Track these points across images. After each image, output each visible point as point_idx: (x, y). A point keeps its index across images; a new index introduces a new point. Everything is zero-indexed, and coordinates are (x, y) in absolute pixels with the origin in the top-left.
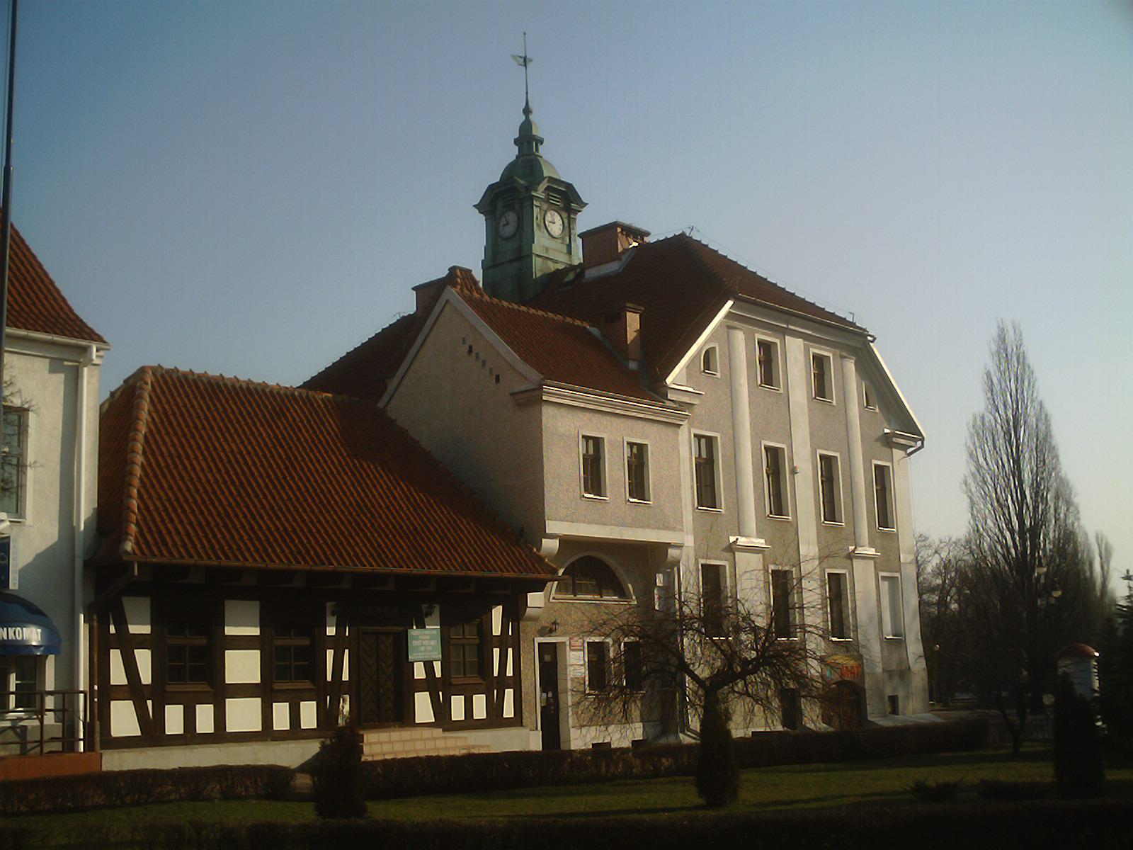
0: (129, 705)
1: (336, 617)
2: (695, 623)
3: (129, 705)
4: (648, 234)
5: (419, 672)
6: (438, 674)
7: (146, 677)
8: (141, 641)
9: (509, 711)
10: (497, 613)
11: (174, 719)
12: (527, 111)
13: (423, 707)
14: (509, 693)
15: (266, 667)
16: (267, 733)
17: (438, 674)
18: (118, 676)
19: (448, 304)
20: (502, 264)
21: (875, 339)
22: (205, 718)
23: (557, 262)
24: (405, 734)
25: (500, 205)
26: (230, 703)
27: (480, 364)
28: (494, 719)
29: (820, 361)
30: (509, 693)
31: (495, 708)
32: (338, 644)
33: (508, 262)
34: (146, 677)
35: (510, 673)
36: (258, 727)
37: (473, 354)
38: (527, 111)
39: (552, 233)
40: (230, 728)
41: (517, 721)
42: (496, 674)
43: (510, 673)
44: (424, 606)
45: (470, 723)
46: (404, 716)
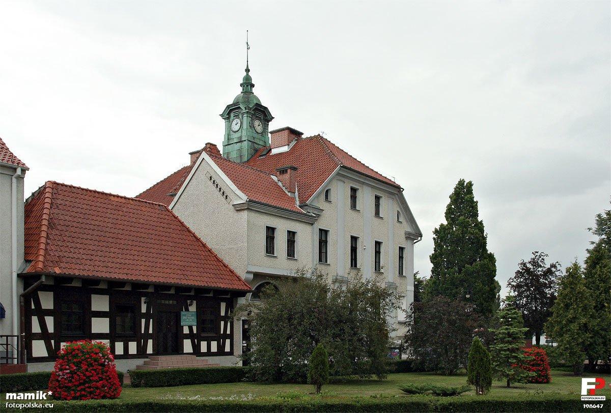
5: (186, 331)
6: (195, 332)
8: (49, 313)
9: (227, 349)
10: (223, 306)
12: (247, 70)
13: (188, 346)
14: (228, 342)
15: (112, 325)
17: (195, 332)
18: (36, 328)
23: (259, 145)
25: (232, 115)
28: (221, 352)
29: (377, 198)
30: (228, 342)
31: (221, 348)
32: (147, 316)
35: (228, 332)
37: (222, 191)
38: (247, 70)
39: (257, 130)
41: (231, 353)
42: (222, 333)
43: (228, 332)
44: (188, 301)
45: (209, 353)
46: (177, 350)
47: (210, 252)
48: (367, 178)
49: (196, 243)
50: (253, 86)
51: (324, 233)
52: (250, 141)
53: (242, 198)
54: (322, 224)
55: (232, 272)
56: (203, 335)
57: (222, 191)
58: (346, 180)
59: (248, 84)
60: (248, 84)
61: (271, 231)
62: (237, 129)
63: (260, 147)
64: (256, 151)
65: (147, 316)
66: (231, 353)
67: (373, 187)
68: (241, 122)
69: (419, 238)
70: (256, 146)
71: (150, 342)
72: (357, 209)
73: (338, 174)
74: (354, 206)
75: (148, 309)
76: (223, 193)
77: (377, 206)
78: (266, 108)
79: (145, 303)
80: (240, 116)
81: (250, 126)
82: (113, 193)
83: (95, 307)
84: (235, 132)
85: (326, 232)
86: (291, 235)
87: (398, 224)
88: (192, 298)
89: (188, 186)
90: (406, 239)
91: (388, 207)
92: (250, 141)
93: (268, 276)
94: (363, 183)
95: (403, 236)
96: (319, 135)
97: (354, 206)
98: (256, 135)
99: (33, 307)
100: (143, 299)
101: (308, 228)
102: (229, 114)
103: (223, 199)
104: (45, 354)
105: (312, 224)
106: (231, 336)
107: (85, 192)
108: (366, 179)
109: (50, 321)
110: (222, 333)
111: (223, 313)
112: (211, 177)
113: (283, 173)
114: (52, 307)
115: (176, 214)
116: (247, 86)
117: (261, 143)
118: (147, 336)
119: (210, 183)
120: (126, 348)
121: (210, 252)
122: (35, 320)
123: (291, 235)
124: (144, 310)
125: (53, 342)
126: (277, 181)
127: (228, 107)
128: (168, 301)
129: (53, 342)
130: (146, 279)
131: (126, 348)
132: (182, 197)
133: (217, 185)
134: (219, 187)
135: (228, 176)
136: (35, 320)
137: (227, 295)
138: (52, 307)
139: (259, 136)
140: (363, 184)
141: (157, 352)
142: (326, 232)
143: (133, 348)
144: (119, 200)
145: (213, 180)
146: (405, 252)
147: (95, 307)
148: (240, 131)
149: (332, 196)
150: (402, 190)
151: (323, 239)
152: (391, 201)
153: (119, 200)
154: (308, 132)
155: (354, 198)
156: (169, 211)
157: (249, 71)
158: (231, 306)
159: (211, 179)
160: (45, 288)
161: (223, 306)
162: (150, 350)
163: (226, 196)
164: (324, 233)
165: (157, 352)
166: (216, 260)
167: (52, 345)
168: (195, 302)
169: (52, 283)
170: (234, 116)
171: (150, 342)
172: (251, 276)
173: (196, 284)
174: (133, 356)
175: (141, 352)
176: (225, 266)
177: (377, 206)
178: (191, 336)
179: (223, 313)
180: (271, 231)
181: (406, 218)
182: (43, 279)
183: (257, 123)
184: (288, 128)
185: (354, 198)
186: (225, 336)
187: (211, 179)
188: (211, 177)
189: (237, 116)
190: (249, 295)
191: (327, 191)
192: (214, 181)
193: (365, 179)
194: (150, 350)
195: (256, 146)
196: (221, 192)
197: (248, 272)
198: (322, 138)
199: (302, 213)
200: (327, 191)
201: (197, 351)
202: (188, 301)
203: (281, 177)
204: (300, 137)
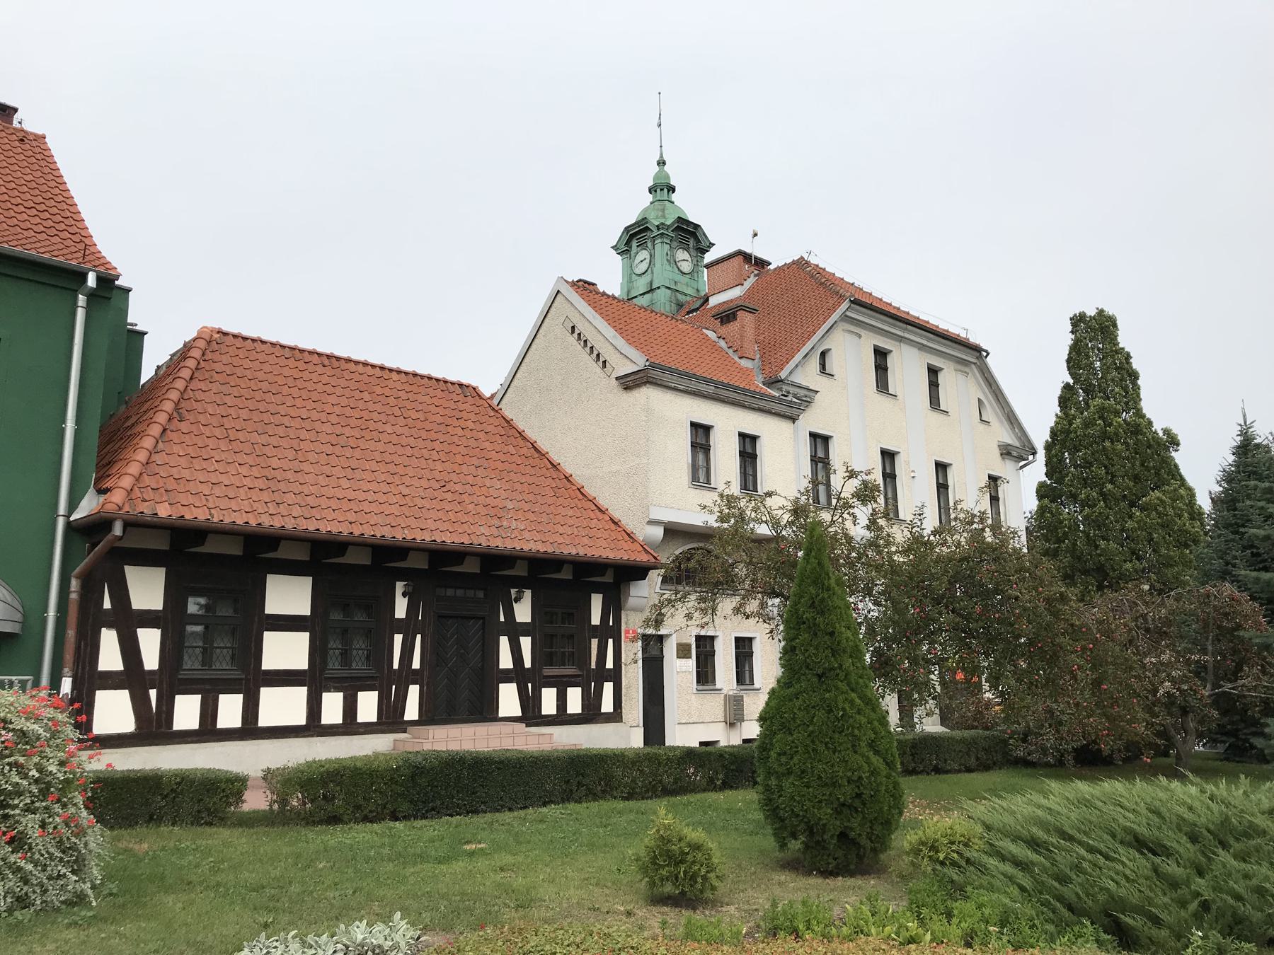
0: (124, 696)
1: (407, 598)
2: (1268, 929)
3: (124, 696)
4: (770, 264)
7: (504, 642)
8: (148, 619)
9: (607, 706)
10: (597, 602)
11: (187, 712)
12: (662, 163)
13: (509, 699)
14: (608, 687)
15: (315, 651)
16: (313, 727)
18: (110, 657)
19: (559, 295)
20: (636, 297)
21: (988, 354)
22: (230, 710)
23: (686, 295)
24: (493, 728)
25: (634, 244)
26: (301, 693)
27: (588, 349)
28: (591, 714)
29: (933, 372)
30: (608, 687)
32: (407, 626)
33: (641, 295)
34: (504, 642)
35: (609, 664)
36: (300, 719)
37: (595, 353)
38: (662, 163)
39: (682, 269)
40: (264, 720)
41: (616, 716)
42: (593, 665)
43: (609, 664)
44: (513, 591)
45: (560, 717)
46: (485, 710)
47: (569, 481)
48: (909, 327)
49: (537, 461)
50: (672, 189)
51: (820, 440)
52: (667, 288)
53: (630, 360)
54: (812, 421)
55: (615, 523)
56: (548, 671)
57: (595, 353)
58: (862, 332)
59: (663, 188)
60: (663, 188)
61: (701, 432)
62: (643, 271)
63: (688, 298)
64: (680, 305)
65: (407, 626)
66: (616, 716)
67: (922, 347)
68: (651, 256)
69: (1031, 457)
70: (680, 297)
71: (414, 692)
72: (890, 392)
73: (845, 318)
74: (882, 384)
75: (411, 609)
76: (598, 355)
77: (934, 385)
78: (697, 226)
79: (404, 595)
80: (649, 244)
81: (668, 260)
82: (355, 357)
83: (274, 605)
84: (640, 275)
85: (826, 439)
86: (748, 444)
87: (982, 427)
88: (521, 584)
89: (530, 352)
90: (1003, 458)
91: (956, 385)
92: (667, 288)
93: (1047, 765)
94: (901, 339)
95: (997, 452)
96: (802, 258)
97: (882, 384)
98: (679, 277)
99: (107, 604)
100: (400, 587)
101: (783, 426)
102: (628, 243)
103: (597, 368)
104: (127, 724)
105: (793, 419)
106: (615, 676)
107: (287, 353)
108: (906, 329)
109: (150, 643)
110: (593, 665)
111: (596, 620)
112: (573, 328)
113: (729, 321)
114: (158, 605)
115: (508, 413)
116: (662, 190)
117: (690, 291)
118: (407, 676)
119: (572, 339)
120: (350, 708)
121: (569, 481)
122: (109, 642)
123: (748, 444)
124: (401, 610)
125: (153, 693)
126: (717, 340)
127: (627, 229)
128: (473, 591)
129: (153, 693)
130: (345, 529)
131: (350, 708)
132: (518, 375)
133: (585, 341)
134: (589, 345)
135: (594, 308)
136: (109, 642)
137: (603, 575)
138: (158, 605)
139: (686, 279)
140: (901, 341)
141: (429, 716)
142: (826, 439)
143: (368, 705)
144: (369, 370)
145: (577, 332)
146: (1003, 490)
147: (274, 605)
148: (649, 270)
149: (833, 363)
150: (985, 354)
151: (820, 454)
152: (961, 377)
153: (369, 370)
154: (777, 258)
155: (881, 368)
156: (493, 409)
157: (664, 163)
158: (614, 604)
159: (573, 332)
160: (145, 558)
161: (597, 602)
162: (412, 711)
163: (604, 362)
164: (820, 440)
165: (429, 716)
166: (580, 496)
167: (151, 705)
168: (528, 594)
169: (164, 546)
170: (638, 246)
171: (414, 692)
172: (658, 532)
173: (526, 548)
174: (368, 729)
175: (390, 719)
176: (600, 510)
177: (934, 385)
178: (518, 675)
179: (596, 620)
180: (701, 432)
181: (997, 415)
182: (118, 530)
183: (681, 255)
184: (740, 253)
185: (881, 368)
186: (603, 675)
187: (573, 332)
188: (573, 328)
189: (642, 245)
190: (655, 577)
191: (823, 354)
192: (579, 334)
193: (905, 330)
194: (412, 711)
195: (680, 297)
196: (594, 355)
197: (652, 522)
198: (808, 263)
199: (770, 396)
200: (823, 354)
201: (531, 714)
202: (513, 591)
203: (723, 330)
204: (763, 267)
